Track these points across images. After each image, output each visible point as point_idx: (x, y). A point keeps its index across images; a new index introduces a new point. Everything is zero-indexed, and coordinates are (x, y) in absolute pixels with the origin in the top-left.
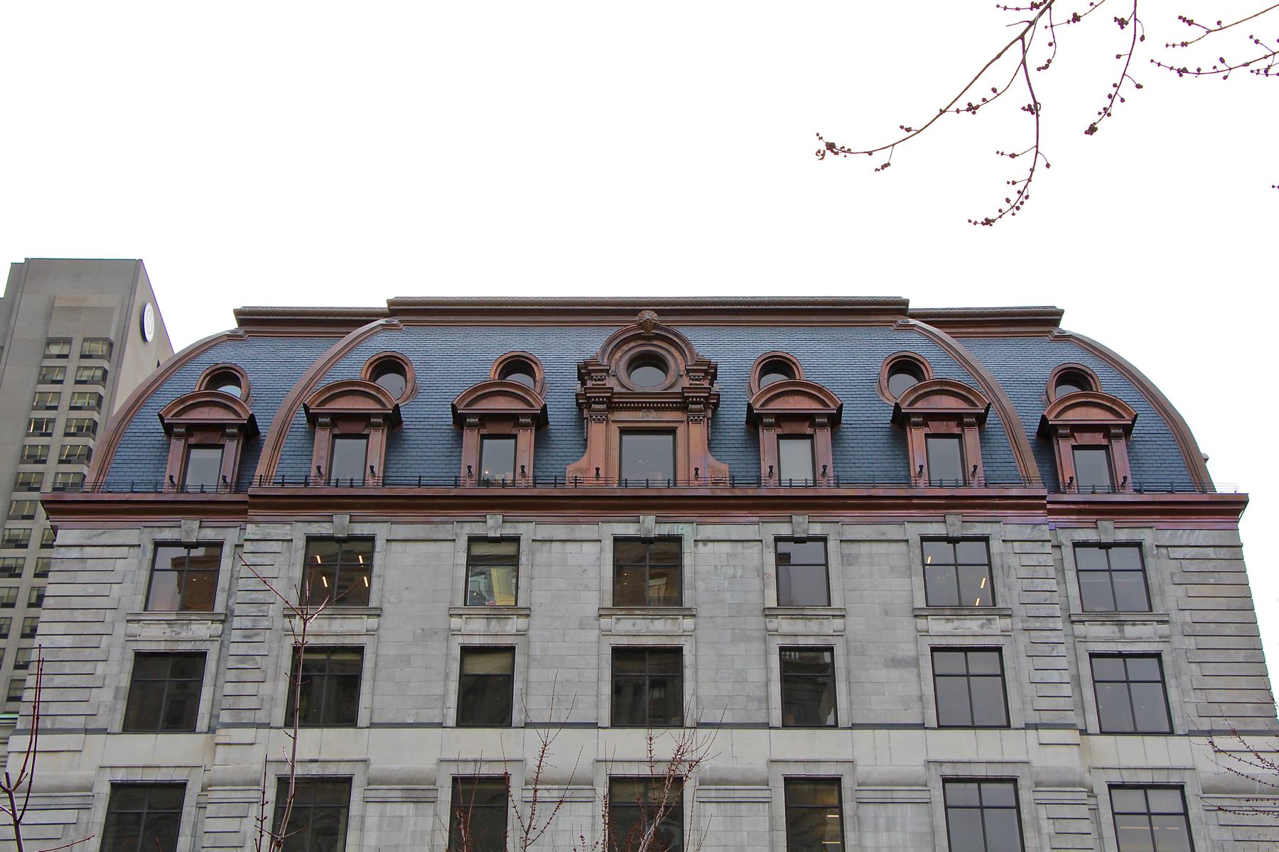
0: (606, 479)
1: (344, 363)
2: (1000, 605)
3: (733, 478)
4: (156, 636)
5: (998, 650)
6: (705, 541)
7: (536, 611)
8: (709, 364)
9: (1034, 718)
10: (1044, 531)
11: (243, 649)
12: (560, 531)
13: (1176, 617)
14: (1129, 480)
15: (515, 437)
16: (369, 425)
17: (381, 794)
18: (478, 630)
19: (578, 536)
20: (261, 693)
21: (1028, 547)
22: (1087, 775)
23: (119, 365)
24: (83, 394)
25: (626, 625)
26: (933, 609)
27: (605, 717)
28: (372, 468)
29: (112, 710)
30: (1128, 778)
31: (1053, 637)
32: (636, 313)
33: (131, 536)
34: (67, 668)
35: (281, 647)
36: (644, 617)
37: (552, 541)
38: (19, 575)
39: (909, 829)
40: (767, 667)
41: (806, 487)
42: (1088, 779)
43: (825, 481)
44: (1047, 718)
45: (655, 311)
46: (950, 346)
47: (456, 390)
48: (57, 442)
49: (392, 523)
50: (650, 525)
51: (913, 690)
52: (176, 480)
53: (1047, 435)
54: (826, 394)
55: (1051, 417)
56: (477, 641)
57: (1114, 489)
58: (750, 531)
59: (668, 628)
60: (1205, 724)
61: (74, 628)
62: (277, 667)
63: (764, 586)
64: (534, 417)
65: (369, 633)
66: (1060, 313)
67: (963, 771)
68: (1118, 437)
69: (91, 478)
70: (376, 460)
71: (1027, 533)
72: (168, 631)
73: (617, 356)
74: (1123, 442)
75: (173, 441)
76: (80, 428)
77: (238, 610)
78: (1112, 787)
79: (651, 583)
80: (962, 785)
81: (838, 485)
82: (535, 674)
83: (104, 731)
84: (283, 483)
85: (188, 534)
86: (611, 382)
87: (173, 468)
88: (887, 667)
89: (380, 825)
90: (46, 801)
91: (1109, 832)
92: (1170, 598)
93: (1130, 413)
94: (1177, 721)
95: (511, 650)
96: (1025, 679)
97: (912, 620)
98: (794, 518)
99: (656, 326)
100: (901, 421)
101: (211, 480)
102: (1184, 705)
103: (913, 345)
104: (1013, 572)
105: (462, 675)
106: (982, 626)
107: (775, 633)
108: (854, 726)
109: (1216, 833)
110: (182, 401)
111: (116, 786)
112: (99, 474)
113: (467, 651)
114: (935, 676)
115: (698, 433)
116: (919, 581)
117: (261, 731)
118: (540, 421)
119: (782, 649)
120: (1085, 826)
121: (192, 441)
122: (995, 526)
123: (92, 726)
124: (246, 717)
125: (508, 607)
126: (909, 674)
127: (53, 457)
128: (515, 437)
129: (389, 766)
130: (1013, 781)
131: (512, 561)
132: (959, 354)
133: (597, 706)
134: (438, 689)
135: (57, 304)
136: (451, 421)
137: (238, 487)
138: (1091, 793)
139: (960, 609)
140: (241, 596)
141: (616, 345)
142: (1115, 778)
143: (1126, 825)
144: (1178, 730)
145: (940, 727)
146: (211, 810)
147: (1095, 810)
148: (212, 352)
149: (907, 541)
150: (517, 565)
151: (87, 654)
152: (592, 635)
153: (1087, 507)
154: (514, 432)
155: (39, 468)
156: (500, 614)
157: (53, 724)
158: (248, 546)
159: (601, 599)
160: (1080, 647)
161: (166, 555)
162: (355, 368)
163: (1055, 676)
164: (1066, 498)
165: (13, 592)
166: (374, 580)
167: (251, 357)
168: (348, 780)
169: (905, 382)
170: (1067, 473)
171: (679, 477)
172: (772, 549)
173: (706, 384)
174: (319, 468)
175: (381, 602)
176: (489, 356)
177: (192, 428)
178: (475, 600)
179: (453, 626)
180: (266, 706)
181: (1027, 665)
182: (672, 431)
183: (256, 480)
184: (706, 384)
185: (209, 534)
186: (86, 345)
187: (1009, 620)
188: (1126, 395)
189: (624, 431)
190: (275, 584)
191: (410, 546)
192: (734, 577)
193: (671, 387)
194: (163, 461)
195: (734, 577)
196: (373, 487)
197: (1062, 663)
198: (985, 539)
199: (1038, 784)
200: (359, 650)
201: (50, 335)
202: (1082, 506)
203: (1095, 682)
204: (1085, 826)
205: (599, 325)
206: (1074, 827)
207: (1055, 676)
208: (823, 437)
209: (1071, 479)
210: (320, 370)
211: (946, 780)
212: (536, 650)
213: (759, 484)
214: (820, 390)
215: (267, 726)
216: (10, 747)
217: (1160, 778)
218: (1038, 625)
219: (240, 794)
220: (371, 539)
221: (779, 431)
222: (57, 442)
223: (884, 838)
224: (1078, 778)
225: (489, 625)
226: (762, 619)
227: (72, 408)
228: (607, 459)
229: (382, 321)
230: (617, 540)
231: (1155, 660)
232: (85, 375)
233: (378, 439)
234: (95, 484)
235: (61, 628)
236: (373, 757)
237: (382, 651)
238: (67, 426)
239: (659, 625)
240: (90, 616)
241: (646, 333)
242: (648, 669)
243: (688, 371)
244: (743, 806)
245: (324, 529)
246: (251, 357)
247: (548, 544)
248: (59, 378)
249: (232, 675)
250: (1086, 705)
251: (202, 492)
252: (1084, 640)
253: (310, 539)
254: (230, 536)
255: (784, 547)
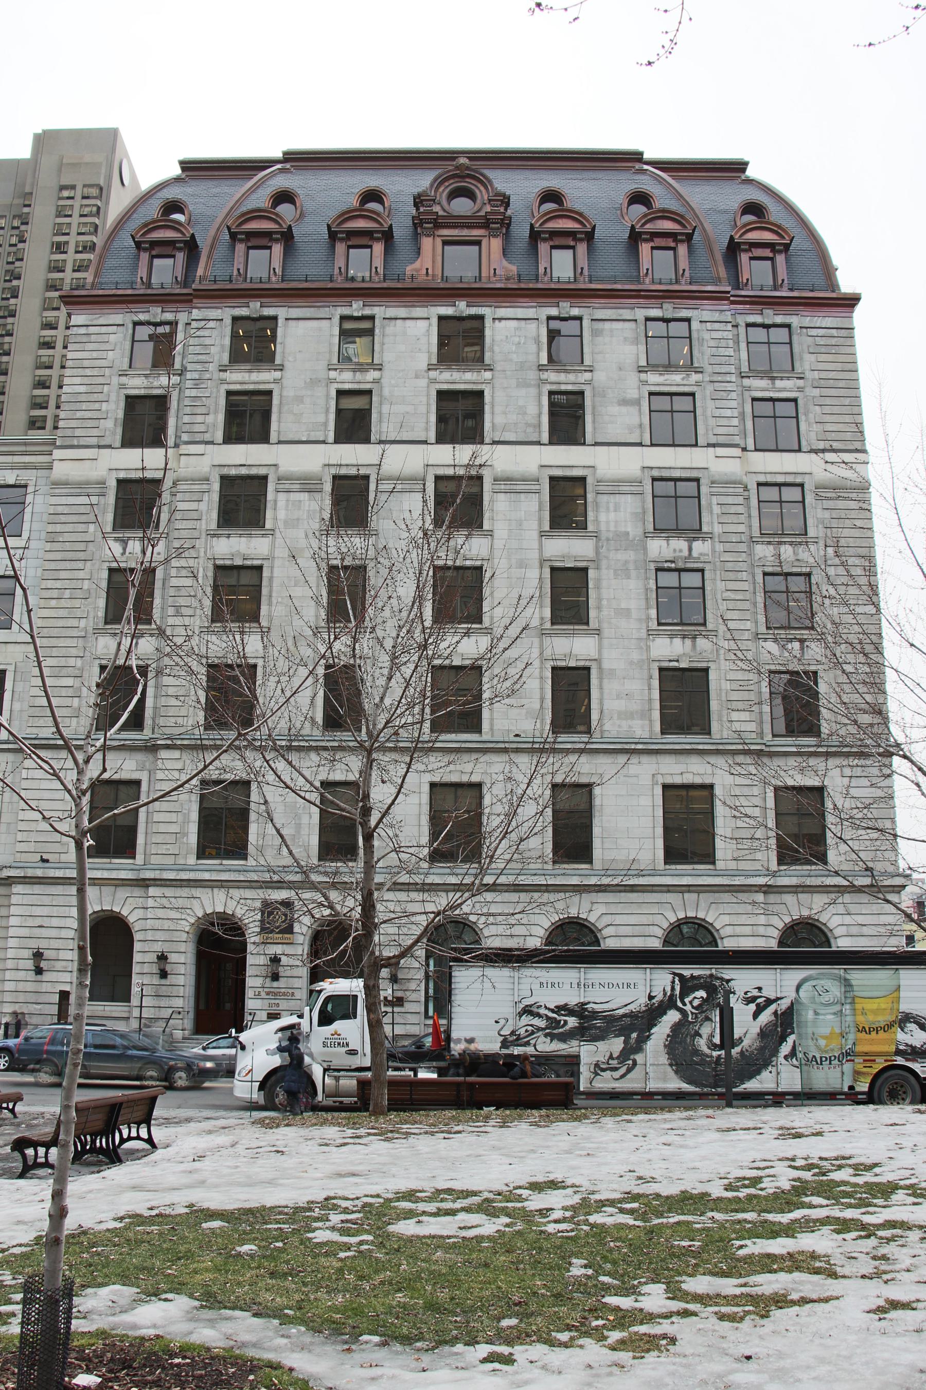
0: (433, 275)
1: (254, 196)
2: (696, 365)
3: (519, 276)
4: (138, 385)
5: (693, 395)
6: (500, 319)
7: (386, 366)
8: (504, 195)
9: (713, 440)
10: (728, 316)
11: (194, 393)
12: (402, 312)
13: (809, 375)
14: (786, 282)
15: (370, 247)
16: (272, 240)
17: (287, 486)
18: (347, 379)
19: (414, 315)
20: (207, 421)
21: (716, 326)
22: (744, 477)
23: (107, 203)
24: (85, 224)
25: (446, 375)
26: (651, 367)
27: (432, 437)
28: (274, 269)
29: (114, 433)
30: (770, 479)
31: (729, 387)
32: (454, 159)
33: (118, 318)
34: (84, 407)
35: (218, 391)
36: (458, 370)
37: (396, 319)
38: (54, 348)
39: (629, 510)
40: (540, 405)
41: (569, 282)
42: (745, 479)
43: (582, 279)
44: (721, 440)
45: (468, 157)
46: (671, 185)
47: (331, 214)
48: (70, 257)
49: (289, 307)
50: (462, 307)
51: (635, 420)
52: (144, 280)
53: (733, 249)
54: (584, 218)
55: (737, 237)
56: (347, 386)
57: (775, 288)
58: (531, 313)
59: (474, 378)
60: (821, 445)
61: (86, 380)
62: (216, 404)
63: (539, 350)
64: (383, 232)
65: (276, 381)
66: (746, 164)
67: (666, 474)
68: (780, 252)
69: (90, 279)
70: (277, 264)
71: (716, 316)
72: (145, 381)
73: (441, 189)
74: (783, 256)
75: (142, 253)
76: (85, 248)
77: (190, 367)
78: (759, 484)
79: (467, 349)
80: (664, 483)
81: (590, 282)
82: (385, 409)
83: (110, 447)
84: (215, 281)
85: (155, 316)
86: (436, 208)
87: (142, 272)
88: (620, 405)
89: (287, 506)
90: (79, 490)
91: (755, 513)
92: (807, 362)
93: (789, 236)
94: (804, 443)
95: (369, 392)
96: (709, 413)
97: (637, 374)
98: (561, 304)
99: (468, 168)
100: (635, 237)
101: (168, 279)
102: (810, 433)
103: (645, 184)
104: (705, 343)
105: (339, 411)
106: (683, 379)
107: (545, 382)
108: (596, 444)
109: (821, 514)
110: (146, 225)
111: (120, 482)
112: (95, 277)
113: (340, 393)
114: (650, 411)
115: (496, 244)
116: (642, 348)
117: (208, 446)
118: (388, 236)
119: (551, 393)
120: (740, 509)
121: (154, 253)
122: (696, 312)
123: (102, 443)
124: (198, 437)
125: (367, 364)
126: (634, 410)
127: (69, 267)
128: (370, 247)
129: (292, 469)
130: (697, 480)
131: (370, 332)
132: (677, 191)
133: (427, 430)
134: (321, 418)
135: (65, 161)
136: (327, 236)
137: (186, 283)
138: (746, 488)
139: (669, 367)
140: (191, 358)
141: (439, 182)
142: (762, 479)
143: (767, 509)
144: (804, 449)
145: (652, 445)
146: (179, 496)
147: (747, 499)
148: (165, 190)
149: (636, 320)
150: (373, 335)
151: (95, 397)
152: (423, 382)
153: (757, 299)
154: (370, 243)
155: (60, 275)
156: (361, 368)
157: (78, 441)
158: (194, 324)
159: (430, 358)
160: (747, 394)
161: (144, 332)
162: (261, 199)
163: (728, 413)
164: (743, 293)
165: (51, 358)
166: (278, 346)
167: (192, 194)
168: (265, 478)
169: (639, 209)
170: (745, 276)
171: (483, 275)
172: (545, 325)
173: (502, 210)
174: (238, 270)
175: (283, 361)
176: (353, 190)
177: (154, 244)
178: (344, 359)
179: (331, 377)
180: (211, 430)
181: (711, 404)
182: (478, 243)
183: (197, 279)
184: (502, 210)
185: (169, 316)
186: (85, 190)
187: (700, 375)
188: (787, 223)
189: (445, 243)
190: (213, 350)
191: (301, 322)
192: (519, 343)
193: (478, 211)
194: (135, 267)
195: (519, 343)
196: (275, 282)
197: (734, 404)
198: (688, 320)
199: (712, 483)
200: (269, 393)
201: (62, 183)
202: (753, 299)
203: (754, 417)
204: (740, 509)
205: (430, 168)
206: (733, 509)
207: (728, 413)
208: (582, 248)
209: (748, 280)
210: (237, 201)
211: (654, 479)
212: (386, 392)
213: (537, 280)
214: (581, 214)
215: (212, 443)
216: (54, 457)
217: (790, 479)
218: (720, 379)
219: (196, 487)
220: (275, 318)
221: (552, 243)
222: (70, 257)
223: (612, 515)
224: (738, 478)
225: (354, 376)
226: (537, 372)
227: (79, 234)
228: (433, 262)
229: (279, 166)
230: (441, 318)
231: (793, 404)
232: (86, 210)
233: (277, 249)
234: (93, 283)
235: (78, 380)
236: (280, 463)
237: (285, 393)
238: (77, 246)
239: (468, 376)
240: (95, 372)
241: (462, 174)
242: (462, 405)
243: (490, 200)
244: (522, 495)
245: (244, 312)
246: (192, 194)
247: (393, 321)
248: (70, 213)
249: (188, 410)
250: (747, 432)
251: (162, 288)
252: (749, 389)
253: (235, 319)
254: (182, 318)
255: (555, 325)
